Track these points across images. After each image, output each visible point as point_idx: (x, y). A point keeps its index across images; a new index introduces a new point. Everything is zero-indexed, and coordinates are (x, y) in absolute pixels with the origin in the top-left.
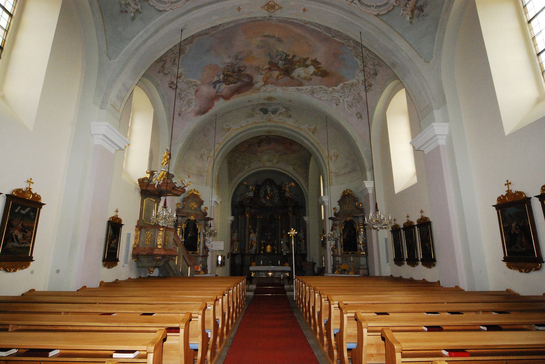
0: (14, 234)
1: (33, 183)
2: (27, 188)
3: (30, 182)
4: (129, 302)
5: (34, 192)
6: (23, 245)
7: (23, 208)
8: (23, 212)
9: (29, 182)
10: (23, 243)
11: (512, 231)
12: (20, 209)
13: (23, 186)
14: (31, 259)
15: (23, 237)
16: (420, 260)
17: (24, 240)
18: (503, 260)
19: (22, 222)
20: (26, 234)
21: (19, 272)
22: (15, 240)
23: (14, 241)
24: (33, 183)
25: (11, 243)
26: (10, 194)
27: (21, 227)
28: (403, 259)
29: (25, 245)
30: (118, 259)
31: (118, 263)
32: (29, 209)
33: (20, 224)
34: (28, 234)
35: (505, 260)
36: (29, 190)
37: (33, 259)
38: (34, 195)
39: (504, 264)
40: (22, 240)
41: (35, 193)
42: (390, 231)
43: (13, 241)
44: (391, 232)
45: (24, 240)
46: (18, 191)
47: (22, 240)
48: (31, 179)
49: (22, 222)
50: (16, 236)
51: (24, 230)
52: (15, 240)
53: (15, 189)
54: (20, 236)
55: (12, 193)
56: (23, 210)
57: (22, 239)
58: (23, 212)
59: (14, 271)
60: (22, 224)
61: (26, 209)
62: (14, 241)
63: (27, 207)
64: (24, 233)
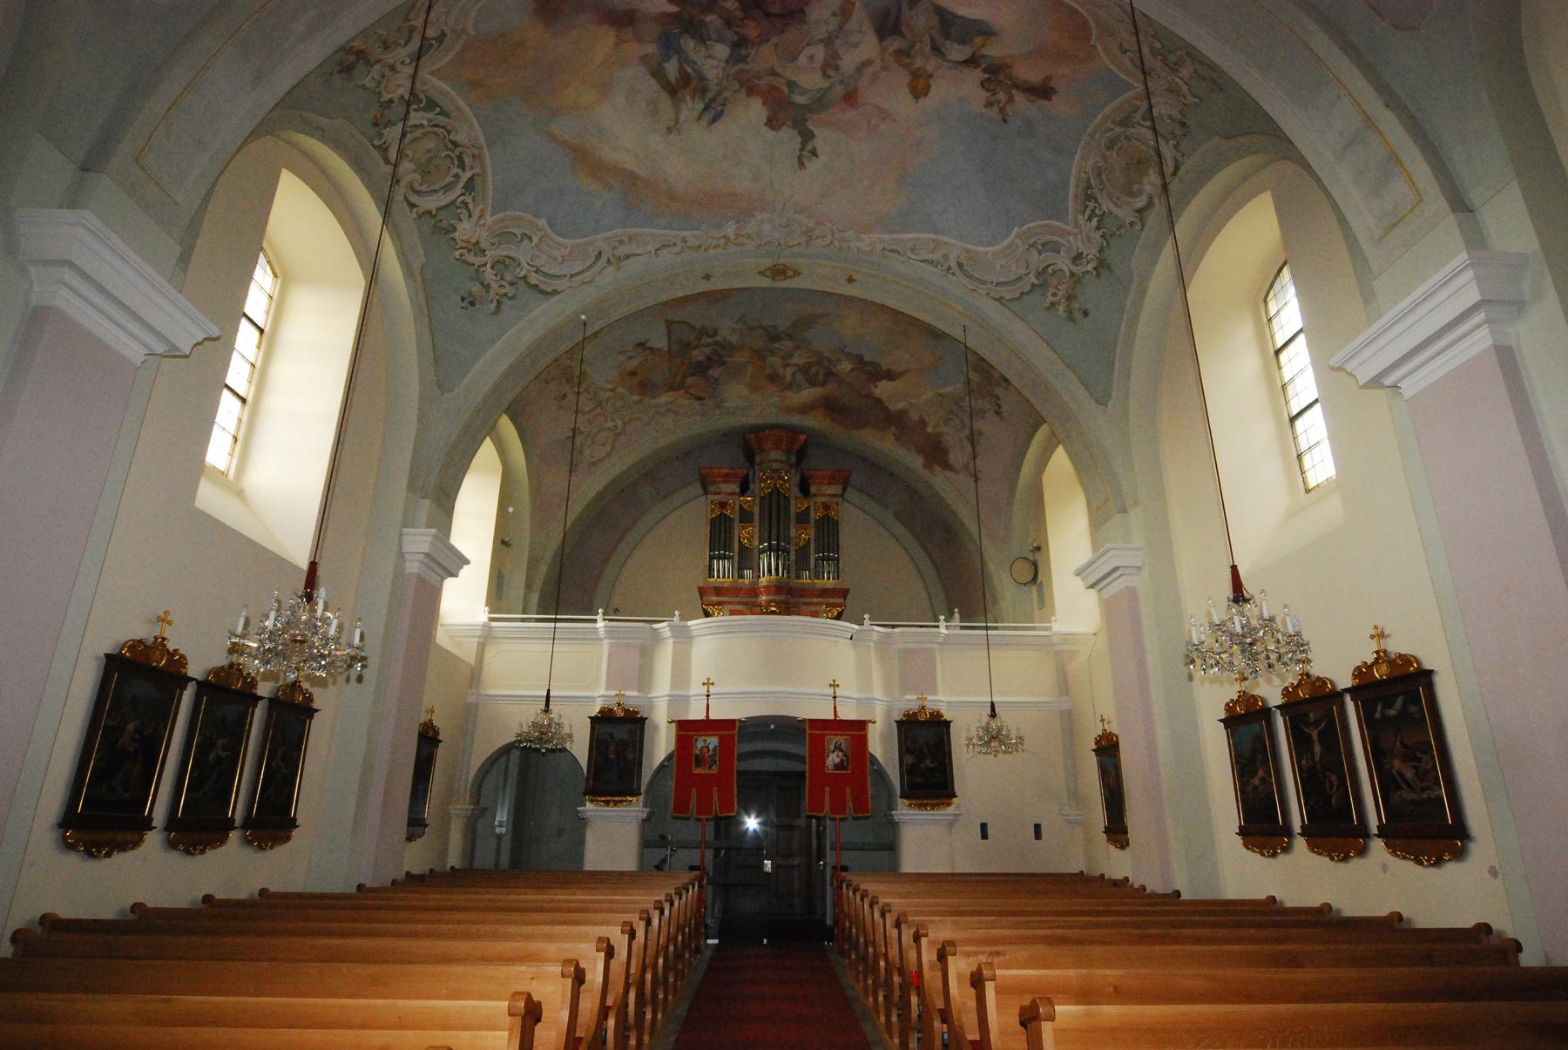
0: (1394, 771)
1: (170, 623)
2: (156, 638)
3: (163, 620)
4: (882, 931)
5: (171, 646)
6: (1425, 796)
7: (1389, 704)
8: (1392, 712)
9: (163, 620)
10: (1423, 790)
11: (120, 743)
12: (1384, 708)
13: (142, 631)
14: (293, 824)
15: (1417, 774)
16: (1375, 831)
17: (1422, 781)
18: (1238, 831)
19: (1398, 738)
20: (1421, 765)
21: (119, 858)
22: (1404, 786)
23: (1402, 788)
24: (170, 623)
25: (1398, 793)
26: (114, 653)
27: (1403, 750)
28: (1287, 831)
29: (1429, 794)
30: (294, 819)
31: (295, 833)
32: (1400, 701)
33: (1398, 743)
34: (1427, 764)
35: (1243, 832)
36: (160, 642)
37: (153, 825)
38: (171, 655)
39: (1239, 839)
40: (1417, 783)
41: (174, 650)
42: (1093, 750)
43: (1399, 788)
44: (1094, 753)
45: (1422, 781)
46: (135, 645)
47: (1417, 783)
48: (1376, 627)
49: (1398, 738)
50: (1401, 775)
51: (1410, 756)
52: (1404, 786)
53: (129, 641)
54: (1409, 774)
55: (118, 651)
56: (1391, 708)
57: (1415, 778)
58: (1392, 712)
59: (202, 852)
60: (1401, 743)
61: (1395, 702)
62: (1402, 788)
63: (1395, 696)
64: (1416, 764)
